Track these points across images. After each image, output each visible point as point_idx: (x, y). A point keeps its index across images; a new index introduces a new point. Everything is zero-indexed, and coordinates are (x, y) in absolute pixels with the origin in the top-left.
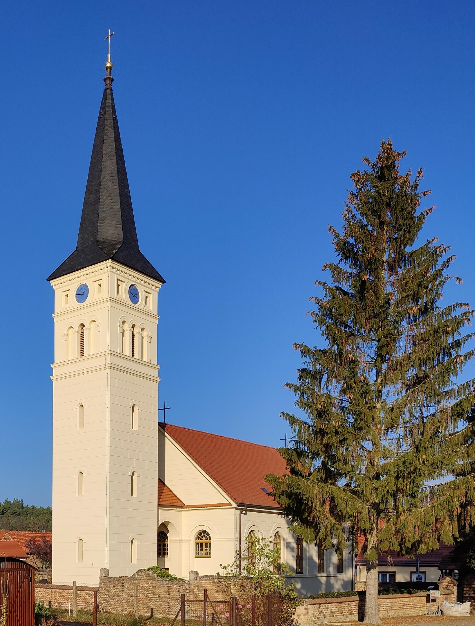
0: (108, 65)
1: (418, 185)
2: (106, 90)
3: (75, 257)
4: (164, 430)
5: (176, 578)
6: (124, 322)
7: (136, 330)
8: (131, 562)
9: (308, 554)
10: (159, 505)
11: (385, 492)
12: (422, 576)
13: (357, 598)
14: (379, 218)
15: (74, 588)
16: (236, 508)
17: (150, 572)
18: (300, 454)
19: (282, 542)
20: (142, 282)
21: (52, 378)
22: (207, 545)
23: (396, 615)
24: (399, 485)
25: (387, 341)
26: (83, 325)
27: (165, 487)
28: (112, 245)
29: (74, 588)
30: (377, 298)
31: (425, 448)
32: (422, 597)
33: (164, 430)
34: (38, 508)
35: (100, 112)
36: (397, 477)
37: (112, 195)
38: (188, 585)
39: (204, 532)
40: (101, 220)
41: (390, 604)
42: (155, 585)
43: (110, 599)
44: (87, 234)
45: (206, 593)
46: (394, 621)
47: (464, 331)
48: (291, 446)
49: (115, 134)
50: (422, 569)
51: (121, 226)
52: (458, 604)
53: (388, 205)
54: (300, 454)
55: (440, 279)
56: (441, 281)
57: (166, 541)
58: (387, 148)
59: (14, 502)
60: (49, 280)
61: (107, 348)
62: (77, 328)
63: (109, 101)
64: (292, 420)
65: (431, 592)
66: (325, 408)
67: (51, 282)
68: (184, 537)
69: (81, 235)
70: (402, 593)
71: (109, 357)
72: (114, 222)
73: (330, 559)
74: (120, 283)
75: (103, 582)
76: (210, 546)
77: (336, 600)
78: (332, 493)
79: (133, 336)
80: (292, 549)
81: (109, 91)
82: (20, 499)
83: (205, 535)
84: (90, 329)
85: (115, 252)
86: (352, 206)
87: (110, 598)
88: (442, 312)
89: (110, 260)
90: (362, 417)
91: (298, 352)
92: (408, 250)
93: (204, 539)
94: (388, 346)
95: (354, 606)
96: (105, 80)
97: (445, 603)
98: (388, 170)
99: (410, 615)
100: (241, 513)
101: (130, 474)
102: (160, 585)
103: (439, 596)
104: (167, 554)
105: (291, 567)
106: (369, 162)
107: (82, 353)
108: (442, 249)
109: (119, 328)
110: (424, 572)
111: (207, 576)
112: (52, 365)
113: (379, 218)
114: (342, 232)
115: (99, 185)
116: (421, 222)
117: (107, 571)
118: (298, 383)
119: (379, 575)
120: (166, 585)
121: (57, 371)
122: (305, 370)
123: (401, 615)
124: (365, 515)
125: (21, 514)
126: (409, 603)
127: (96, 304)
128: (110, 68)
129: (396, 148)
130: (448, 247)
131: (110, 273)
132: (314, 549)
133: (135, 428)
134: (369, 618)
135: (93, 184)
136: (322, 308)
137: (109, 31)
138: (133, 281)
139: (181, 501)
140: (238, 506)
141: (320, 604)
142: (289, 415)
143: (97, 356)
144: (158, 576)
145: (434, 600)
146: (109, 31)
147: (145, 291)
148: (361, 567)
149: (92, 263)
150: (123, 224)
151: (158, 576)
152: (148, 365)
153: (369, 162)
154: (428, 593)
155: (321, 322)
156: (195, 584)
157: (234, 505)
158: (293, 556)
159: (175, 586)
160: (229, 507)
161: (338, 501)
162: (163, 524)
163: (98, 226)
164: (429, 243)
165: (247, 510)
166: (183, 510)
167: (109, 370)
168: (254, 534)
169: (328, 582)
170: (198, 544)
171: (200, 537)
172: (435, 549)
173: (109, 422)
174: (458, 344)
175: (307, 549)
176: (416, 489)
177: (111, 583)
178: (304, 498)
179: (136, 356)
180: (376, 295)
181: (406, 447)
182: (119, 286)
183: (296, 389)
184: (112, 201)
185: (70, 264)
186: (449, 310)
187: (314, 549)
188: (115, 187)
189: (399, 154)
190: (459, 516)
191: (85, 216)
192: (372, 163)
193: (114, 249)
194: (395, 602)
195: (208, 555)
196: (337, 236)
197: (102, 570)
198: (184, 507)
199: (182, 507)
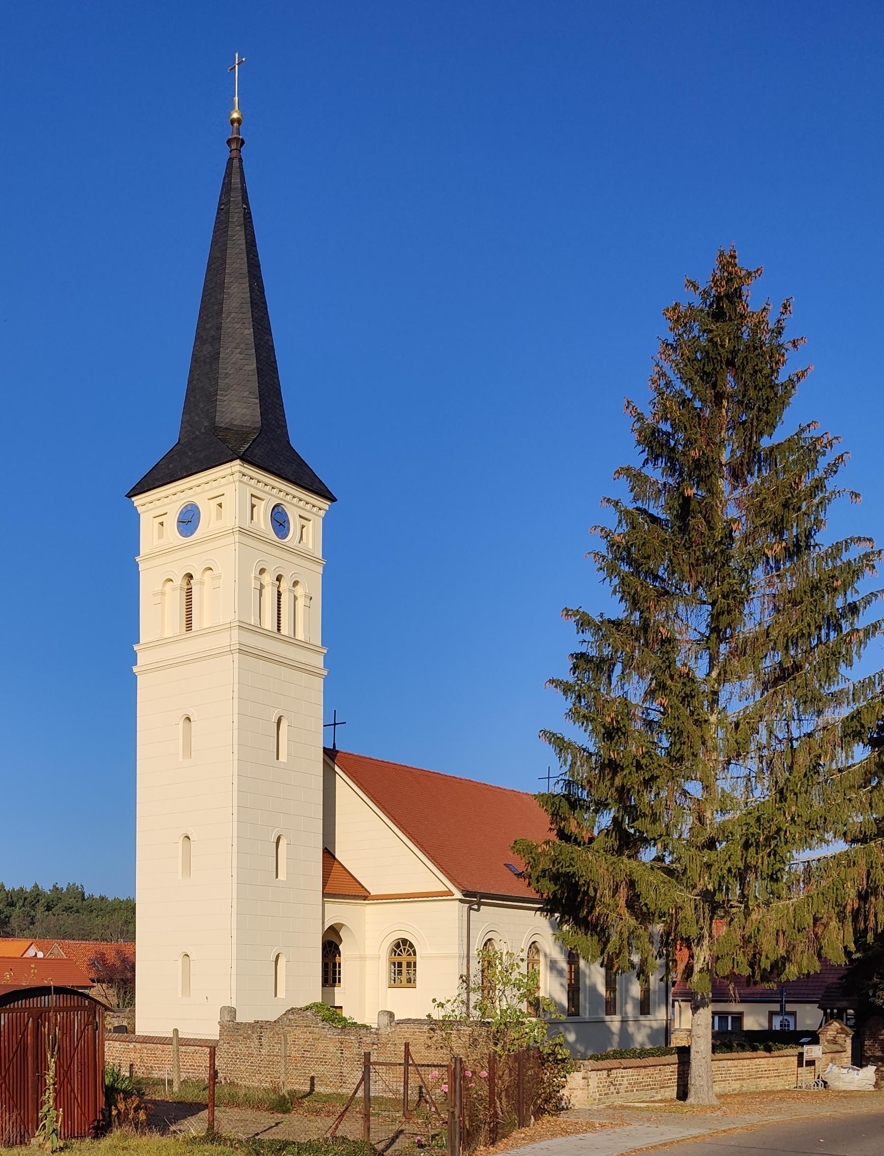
0: (235, 115)
2: (231, 160)
3: (176, 456)
4: (334, 761)
5: (356, 1023)
6: (262, 571)
7: (285, 585)
8: (276, 996)
9: (588, 982)
10: (325, 895)
11: (725, 871)
12: (791, 1020)
13: (675, 1058)
14: (714, 386)
15: (175, 1042)
18: (574, 804)
22: (409, 965)
23: (744, 1089)
24: (749, 859)
26: (190, 576)
27: (336, 863)
28: (242, 434)
29: (175, 1042)
30: (711, 528)
31: (796, 794)
32: (789, 1058)
34: (110, 899)
36: (746, 846)
37: (242, 346)
38: (375, 1036)
39: (405, 941)
41: (733, 1070)
43: (238, 1060)
44: (198, 415)
45: (409, 1050)
46: (740, 1099)
47: (864, 586)
50: (789, 1007)
51: (258, 401)
53: (730, 363)
54: (574, 804)
55: (821, 495)
56: (823, 498)
57: (337, 957)
58: (728, 263)
59: (67, 889)
60: (130, 496)
62: (179, 581)
63: (236, 180)
64: (560, 744)
65: (806, 1048)
66: (618, 722)
67: (133, 499)
70: (755, 1049)
71: (235, 631)
72: (246, 394)
73: (627, 990)
74: (255, 501)
76: (415, 966)
78: (631, 873)
79: (279, 594)
80: (560, 973)
81: (236, 162)
82: (78, 884)
83: (407, 947)
84: (202, 583)
85: (247, 446)
86: (666, 366)
89: (238, 462)
92: (766, 442)
93: (404, 955)
94: (729, 613)
95: (670, 1072)
96: (229, 142)
97: (831, 1068)
98: (730, 302)
99: (768, 1089)
100: (470, 908)
102: (326, 1037)
104: (339, 982)
105: (558, 1005)
106: (696, 288)
107: (189, 627)
108: (825, 441)
109: (253, 581)
110: (793, 1014)
112: (136, 648)
113: (714, 386)
114: (648, 412)
115: (219, 328)
116: (788, 394)
117: (232, 1012)
118: (571, 679)
119: (713, 1018)
121: (144, 658)
122: (583, 655)
123: (753, 1088)
124: (689, 912)
126: (766, 1067)
128: (239, 121)
129: (744, 263)
130: (837, 438)
131: (237, 483)
132: (599, 972)
133: (283, 758)
134: (696, 1094)
135: (208, 326)
136: (613, 545)
137: (237, 55)
139: (363, 887)
140: (464, 895)
141: (610, 1070)
143: (215, 630)
144: (323, 1021)
145: (811, 1063)
146: (237, 55)
147: (300, 517)
148: (682, 1004)
149: (206, 466)
150: (262, 398)
151: (323, 1021)
152: (304, 646)
153: (696, 288)
154: (800, 1049)
155: (612, 570)
156: (388, 1035)
157: (458, 895)
158: (562, 985)
159: (352, 1038)
161: (641, 888)
163: (216, 400)
164: (803, 430)
165: (480, 904)
167: (236, 655)
168: (492, 945)
170: (394, 964)
171: (398, 951)
172: (812, 973)
174: (853, 609)
175: (587, 972)
177: (241, 1032)
178: (581, 882)
179: (285, 630)
180: (708, 522)
181: (762, 792)
182: (253, 506)
183: (567, 689)
184: (242, 356)
185: (168, 467)
186: (837, 549)
187: (599, 972)
188: (247, 332)
189: (749, 274)
191: (194, 382)
192: (701, 289)
193: (245, 441)
194: (743, 1066)
195: (411, 982)
196: (640, 418)
198: (369, 898)
199: (365, 898)
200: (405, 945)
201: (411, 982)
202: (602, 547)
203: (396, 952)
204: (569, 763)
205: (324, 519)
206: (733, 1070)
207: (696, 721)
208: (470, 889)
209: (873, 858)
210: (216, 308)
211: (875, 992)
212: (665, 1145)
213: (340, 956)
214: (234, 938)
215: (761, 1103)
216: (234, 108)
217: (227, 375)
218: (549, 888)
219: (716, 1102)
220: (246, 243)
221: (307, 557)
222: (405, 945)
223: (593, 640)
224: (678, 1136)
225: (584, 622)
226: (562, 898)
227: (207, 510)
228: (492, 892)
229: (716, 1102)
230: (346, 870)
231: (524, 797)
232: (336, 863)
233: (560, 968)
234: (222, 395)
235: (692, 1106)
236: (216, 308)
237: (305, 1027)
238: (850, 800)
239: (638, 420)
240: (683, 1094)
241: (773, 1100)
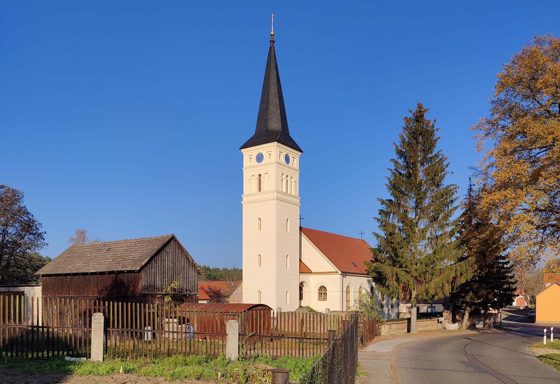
0: (272, 33)
1: (434, 126)
2: (271, 47)
3: (255, 138)
6: (283, 174)
10: (300, 272)
11: (421, 272)
12: (433, 309)
13: (406, 321)
14: (416, 140)
16: (341, 274)
18: (380, 251)
20: (288, 151)
21: (242, 202)
22: (324, 294)
24: (427, 269)
25: (421, 201)
26: (260, 175)
28: (276, 133)
30: (416, 179)
31: (438, 252)
34: (202, 266)
35: (268, 59)
36: (426, 266)
37: (276, 105)
39: (323, 286)
40: (270, 119)
41: (421, 324)
44: (262, 126)
46: (423, 332)
48: (376, 247)
49: (276, 72)
50: (433, 305)
51: (281, 123)
52: (452, 324)
53: (421, 134)
54: (380, 251)
55: (444, 172)
56: (444, 173)
58: (420, 107)
60: (240, 149)
61: (273, 188)
62: (257, 176)
63: (273, 53)
64: (377, 236)
65: (440, 318)
66: (393, 232)
67: (241, 150)
69: (258, 126)
71: (275, 193)
72: (277, 120)
74: (280, 153)
76: (326, 294)
77: (397, 322)
78: (397, 272)
79: (287, 181)
81: (272, 48)
83: (324, 288)
84: (264, 177)
85: (278, 137)
86: (404, 135)
88: (445, 188)
89: (276, 142)
90: (410, 237)
91: (379, 203)
92: (430, 155)
93: (323, 291)
94: (421, 203)
95: (405, 325)
96: (270, 41)
98: (421, 117)
99: (430, 330)
100: (343, 277)
101: (286, 256)
103: (444, 320)
104: (302, 299)
106: (411, 112)
107: (260, 190)
108: (445, 158)
109: (280, 178)
110: (434, 307)
111: (334, 311)
112: (242, 196)
113: (416, 140)
114: (398, 144)
115: (268, 99)
121: (245, 199)
122: (382, 210)
123: (426, 330)
124: (411, 282)
126: (429, 324)
127: (268, 164)
128: (273, 35)
129: (425, 106)
130: (448, 157)
131: (276, 148)
133: (288, 231)
134: (413, 331)
135: (265, 98)
136: (391, 182)
137: (273, 14)
141: (390, 325)
143: (268, 192)
145: (441, 322)
146: (273, 14)
147: (293, 157)
149: (265, 142)
152: (294, 197)
153: (411, 112)
154: (438, 318)
155: (390, 189)
157: (340, 273)
160: (337, 273)
161: (399, 276)
163: (268, 122)
164: (439, 152)
165: (346, 275)
167: (276, 201)
168: (349, 287)
169: (389, 313)
170: (320, 293)
171: (321, 289)
172: (442, 298)
173: (276, 228)
174: (452, 201)
176: (434, 272)
178: (384, 274)
179: (289, 192)
180: (415, 178)
181: (430, 251)
182: (280, 155)
183: (378, 220)
184: (275, 109)
185: (253, 141)
188: (277, 101)
189: (425, 110)
190: (452, 282)
191: (260, 115)
192: (413, 112)
193: (278, 136)
195: (325, 299)
196: (397, 147)
199: (311, 273)
200: (323, 287)
201: (325, 299)
202: (387, 182)
203: (320, 290)
204: (380, 241)
205: (299, 158)
206: (421, 324)
207: (413, 232)
208: (343, 271)
209: (457, 268)
210: (267, 93)
211: (458, 302)
212: (409, 342)
214: (275, 286)
215: (429, 333)
216: (271, 31)
217: (271, 114)
218: (374, 274)
219: (418, 333)
220: (276, 73)
221: (295, 170)
222: (323, 287)
223: (385, 207)
224: (412, 340)
225: (383, 202)
226: (377, 278)
227: (266, 156)
228: (349, 272)
229: (418, 333)
230: (304, 264)
231: (355, 240)
234: (270, 120)
235: (412, 334)
236: (267, 93)
238: (451, 253)
240: (409, 331)
241: (432, 332)
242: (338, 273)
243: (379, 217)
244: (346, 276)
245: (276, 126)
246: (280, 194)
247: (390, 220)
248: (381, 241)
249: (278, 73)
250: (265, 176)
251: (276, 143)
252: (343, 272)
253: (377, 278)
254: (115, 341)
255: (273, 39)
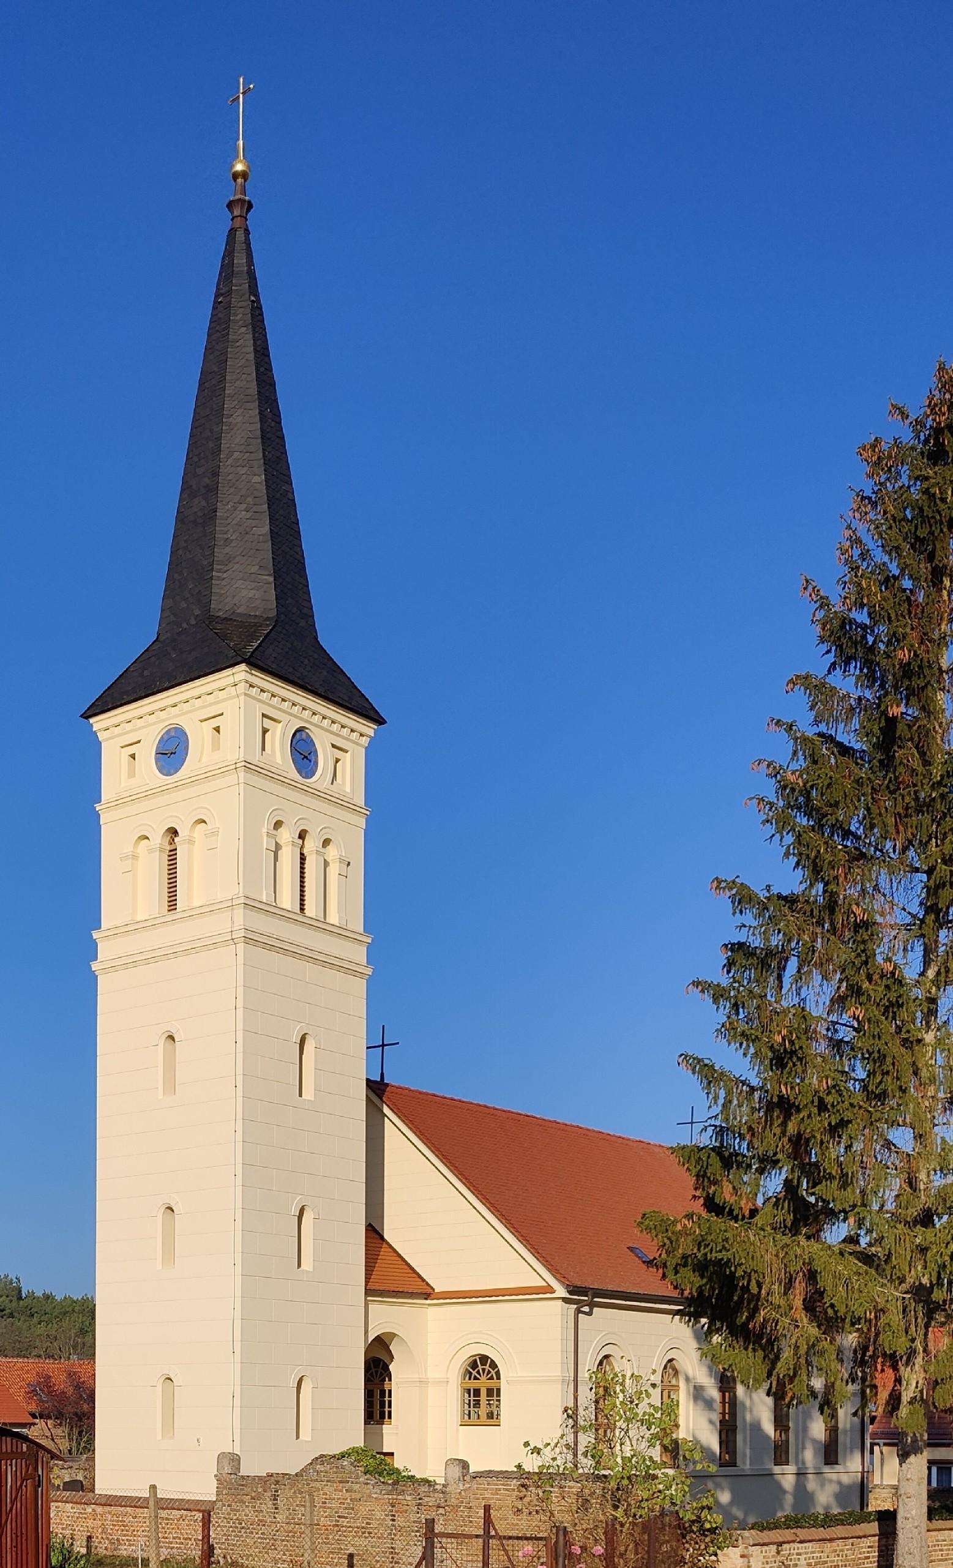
0: (239, 167)
2: (232, 231)
4: (382, 1100)
5: (413, 1477)
6: (278, 825)
7: (311, 845)
8: (298, 1437)
9: (748, 1417)
10: (368, 1292)
13: (874, 1527)
14: (931, 557)
15: (152, 1503)
16: (565, 1300)
17: (345, 1463)
18: (729, 1160)
19: (682, 1384)
20: (326, 721)
21: (95, 966)
22: (490, 1392)
26: (174, 832)
27: (385, 1245)
28: (248, 627)
29: (152, 1503)
30: (926, 763)
33: (382, 1100)
38: (441, 1495)
39: (484, 1359)
42: (358, 1496)
43: (243, 1531)
44: (185, 599)
45: (490, 1515)
49: (255, 344)
51: (271, 579)
54: (729, 1160)
60: (88, 715)
61: (231, 889)
62: (158, 839)
63: (240, 260)
66: (792, 1042)
67: (92, 720)
68: (433, 1374)
71: (239, 912)
72: (255, 569)
73: (805, 1429)
74: (268, 723)
75: (225, 1488)
76: (498, 1395)
77: (821, 1533)
79: (303, 858)
80: (709, 1404)
81: (240, 235)
83: (487, 1367)
84: (191, 842)
85: (255, 645)
87: (243, 1528)
89: (243, 666)
93: (483, 1378)
96: (230, 205)
100: (578, 1311)
102: (370, 1496)
104: (390, 1417)
105: (706, 1451)
106: (904, 415)
107: (172, 904)
112: (95, 935)
113: (931, 557)
114: (835, 594)
115: (216, 474)
119: (929, 1469)
120: (386, 1496)
122: (741, 945)
125: (16, 1314)
128: (244, 175)
132: (765, 1404)
133: (308, 1094)
136: (784, 788)
137: (241, 80)
138: (301, 719)
139: (423, 1280)
141: (780, 1544)
142: (699, 1061)
143: (210, 910)
144: (365, 1473)
146: (241, 80)
147: (333, 746)
148: (885, 1449)
150: (277, 574)
151: (365, 1473)
152: (340, 933)
153: (904, 415)
155: (783, 823)
156: (460, 1493)
157: (561, 1292)
158: (711, 1422)
159: (409, 1498)
160: (548, 1295)
161: (825, 1282)
162: (378, 1339)
165: (592, 1305)
166: (429, 1305)
167: (241, 946)
168: (610, 1364)
170: (469, 1391)
171: (474, 1373)
175: (748, 1403)
177: (247, 1490)
180: (922, 754)
182: (265, 731)
183: (718, 994)
184: (250, 514)
187: (765, 1404)
188: (256, 479)
191: (180, 552)
192: (913, 417)
193: (252, 637)
195: (493, 1417)
196: (824, 603)
197: (221, 1457)
198: (432, 1296)
199: (427, 1296)
202: (769, 789)
204: (721, 1101)
208: (579, 1284)
213: (390, 1380)
218: (692, 1281)
220: (255, 350)
221: (352, 809)
226: (710, 1297)
227: (198, 737)
230: (399, 1256)
232: (385, 1245)
233: (708, 1398)
234: (219, 571)
237: (340, 1482)
239: (821, 607)
242: (553, 1292)
243: (723, 979)
244: (595, 1309)
245: (251, 594)
246: (262, 917)
247: (784, 991)
248: (727, 1103)
249: (266, 348)
250: (196, 835)
251: (240, 672)
252: (574, 1290)
253: (710, 1297)
254: (806, 1542)
255: (244, 193)
